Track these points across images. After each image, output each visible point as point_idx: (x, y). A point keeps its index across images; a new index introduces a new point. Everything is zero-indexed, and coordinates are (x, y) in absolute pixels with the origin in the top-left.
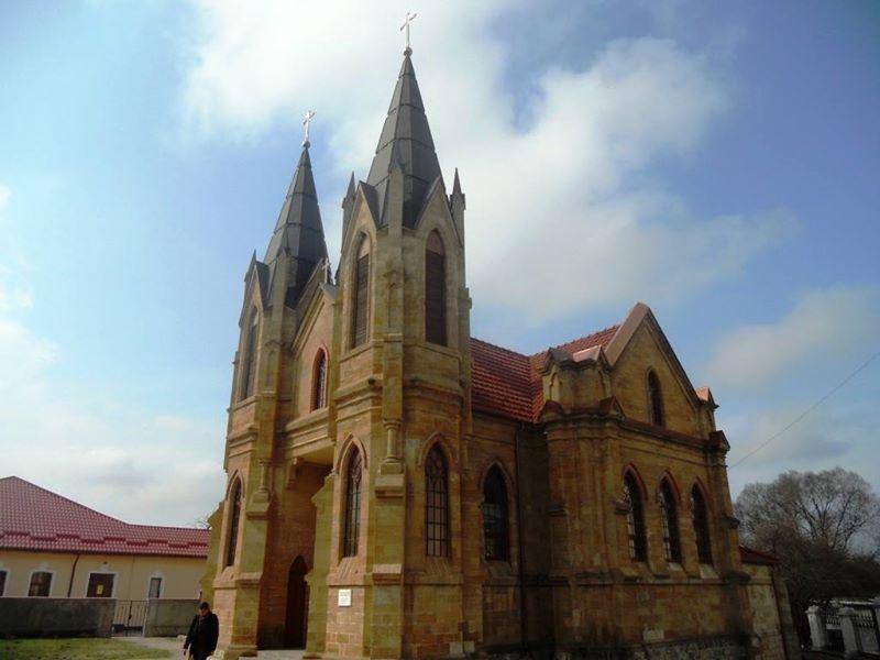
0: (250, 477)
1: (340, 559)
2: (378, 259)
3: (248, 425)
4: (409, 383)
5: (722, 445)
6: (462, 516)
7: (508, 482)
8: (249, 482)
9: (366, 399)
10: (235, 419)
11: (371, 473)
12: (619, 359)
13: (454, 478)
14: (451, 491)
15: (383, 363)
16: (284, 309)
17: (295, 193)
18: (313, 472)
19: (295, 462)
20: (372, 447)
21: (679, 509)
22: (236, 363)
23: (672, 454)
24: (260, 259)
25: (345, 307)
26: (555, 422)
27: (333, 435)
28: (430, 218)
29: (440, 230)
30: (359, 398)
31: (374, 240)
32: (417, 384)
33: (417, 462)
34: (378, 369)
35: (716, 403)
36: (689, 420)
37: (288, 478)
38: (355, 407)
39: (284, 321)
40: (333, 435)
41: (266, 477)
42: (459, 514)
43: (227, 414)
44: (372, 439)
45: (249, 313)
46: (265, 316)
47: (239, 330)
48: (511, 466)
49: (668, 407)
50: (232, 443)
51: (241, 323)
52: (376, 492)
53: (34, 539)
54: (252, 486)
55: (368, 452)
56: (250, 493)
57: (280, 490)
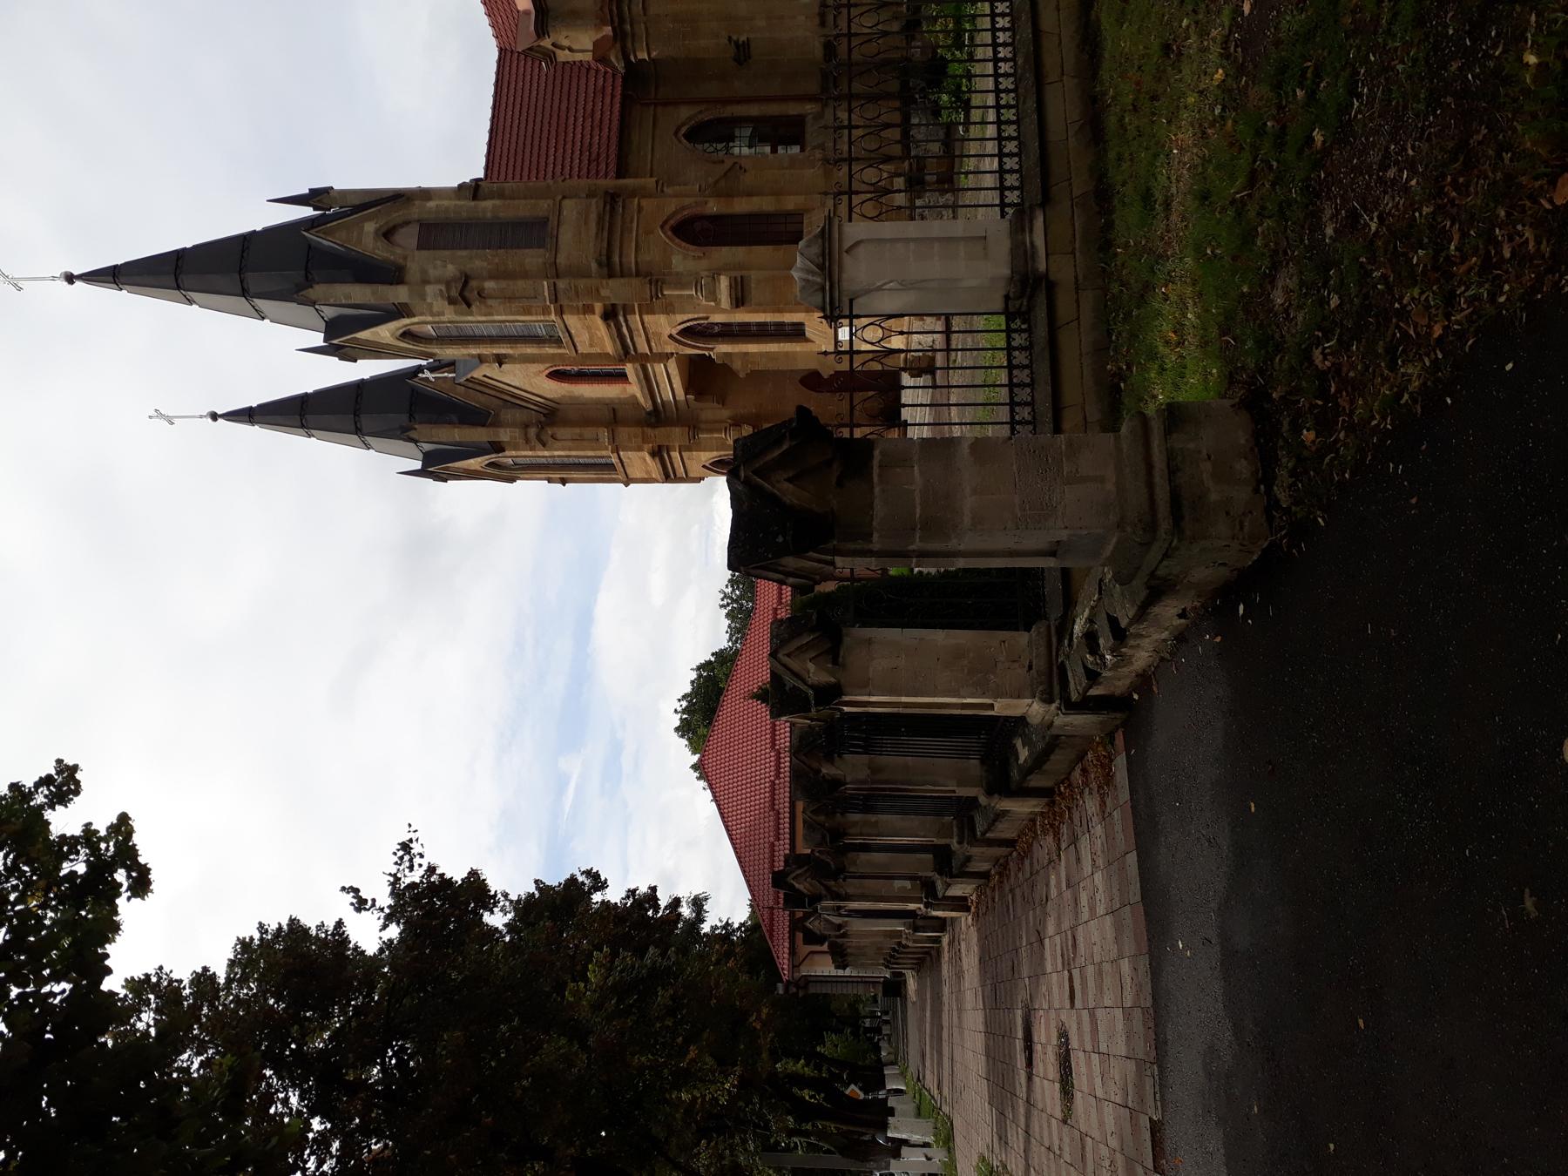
1: (808, 340)
2: (443, 314)
3: (648, 458)
4: (605, 270)
6: (757, 194)
7: (706, 117)
8: (717, 450)
9: (626, 321)
10: (638, 475)
13: (713, 207)
15: (580, 304)
16: (488, 426)
17: (303, 426)
18: (701, 375)
22: (564, 482)
24: (417, 465)
25: (503, 351)
27: (664, 357)
28: (366, 238)
29: (384, 229)
31: (415, 320)
32: (604, 258)
33: (699, 258)
34: (588, 310)
38: (635, 333)
39: (508, 425)
40: (664, 357)
41: (711, 431)
42: (755, 199)
43: (632, 486)
44: (674, 313)
45: (496, 472)
46: (503, 450)
47: (519, 482)
48: (685, 112)
50: (669, 476)
51: (511, 480)
52: (737, 307)
55: (690, 316)
57: (725, 413)
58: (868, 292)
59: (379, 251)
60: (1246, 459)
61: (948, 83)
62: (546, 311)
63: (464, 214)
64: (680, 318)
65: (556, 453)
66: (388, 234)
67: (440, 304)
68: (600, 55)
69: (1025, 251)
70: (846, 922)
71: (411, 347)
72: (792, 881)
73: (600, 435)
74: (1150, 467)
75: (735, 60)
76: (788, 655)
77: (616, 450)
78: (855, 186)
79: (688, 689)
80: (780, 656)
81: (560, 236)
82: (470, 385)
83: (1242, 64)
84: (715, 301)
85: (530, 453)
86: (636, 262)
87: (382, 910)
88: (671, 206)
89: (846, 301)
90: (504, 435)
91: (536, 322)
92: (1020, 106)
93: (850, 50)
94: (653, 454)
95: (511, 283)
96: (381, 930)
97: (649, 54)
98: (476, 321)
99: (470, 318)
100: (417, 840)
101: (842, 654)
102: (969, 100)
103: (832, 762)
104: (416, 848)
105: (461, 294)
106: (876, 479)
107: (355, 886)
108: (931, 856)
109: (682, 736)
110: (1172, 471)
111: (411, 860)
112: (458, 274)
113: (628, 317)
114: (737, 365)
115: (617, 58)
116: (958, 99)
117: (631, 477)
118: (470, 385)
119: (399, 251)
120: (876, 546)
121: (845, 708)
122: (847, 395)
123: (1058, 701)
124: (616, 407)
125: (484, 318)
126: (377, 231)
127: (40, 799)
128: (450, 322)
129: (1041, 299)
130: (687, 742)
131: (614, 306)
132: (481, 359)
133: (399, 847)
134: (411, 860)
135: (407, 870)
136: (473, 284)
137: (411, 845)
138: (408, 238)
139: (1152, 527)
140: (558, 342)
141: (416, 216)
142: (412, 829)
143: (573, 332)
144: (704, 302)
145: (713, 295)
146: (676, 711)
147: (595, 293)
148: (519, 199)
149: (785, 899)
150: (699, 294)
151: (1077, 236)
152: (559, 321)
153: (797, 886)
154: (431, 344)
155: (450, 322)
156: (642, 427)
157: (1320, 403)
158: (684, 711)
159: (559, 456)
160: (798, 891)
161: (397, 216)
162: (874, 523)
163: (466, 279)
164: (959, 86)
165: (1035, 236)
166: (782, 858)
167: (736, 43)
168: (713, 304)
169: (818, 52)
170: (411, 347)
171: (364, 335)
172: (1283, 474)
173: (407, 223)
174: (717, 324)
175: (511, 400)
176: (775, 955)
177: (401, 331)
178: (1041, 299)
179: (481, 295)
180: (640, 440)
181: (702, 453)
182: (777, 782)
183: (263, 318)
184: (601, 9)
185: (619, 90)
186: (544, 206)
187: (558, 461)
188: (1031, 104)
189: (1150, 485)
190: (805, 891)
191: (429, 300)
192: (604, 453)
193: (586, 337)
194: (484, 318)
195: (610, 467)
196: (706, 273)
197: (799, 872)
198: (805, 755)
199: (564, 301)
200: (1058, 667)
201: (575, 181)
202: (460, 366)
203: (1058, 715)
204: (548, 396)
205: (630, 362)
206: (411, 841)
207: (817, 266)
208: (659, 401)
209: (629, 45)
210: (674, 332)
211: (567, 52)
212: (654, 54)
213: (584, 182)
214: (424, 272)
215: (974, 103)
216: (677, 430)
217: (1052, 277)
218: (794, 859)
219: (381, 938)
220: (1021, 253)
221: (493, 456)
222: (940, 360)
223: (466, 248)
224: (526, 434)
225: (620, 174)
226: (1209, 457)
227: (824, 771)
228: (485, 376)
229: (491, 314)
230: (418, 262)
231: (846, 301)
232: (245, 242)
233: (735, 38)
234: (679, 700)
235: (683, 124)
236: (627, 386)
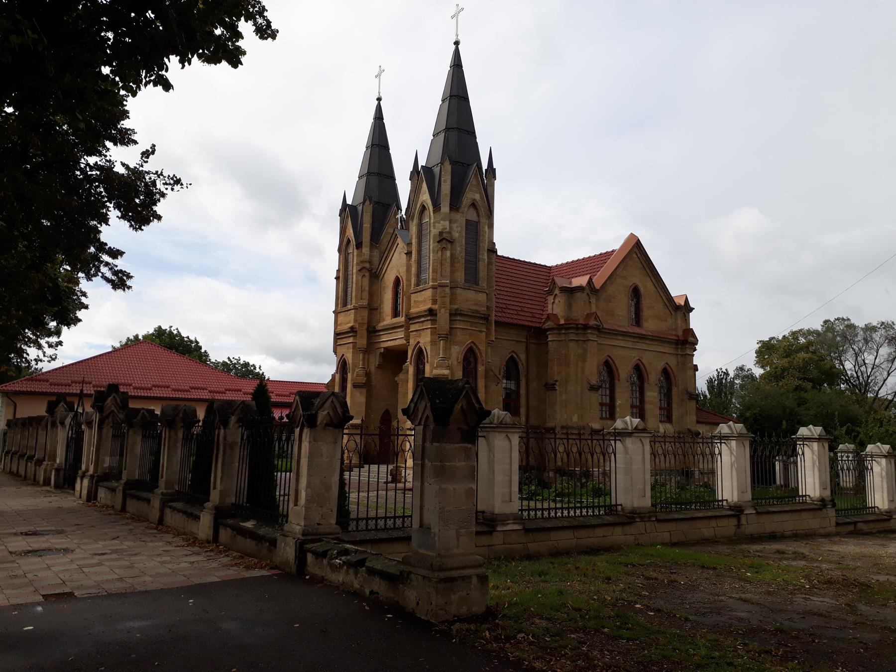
0: (353, 360)
2: (434, 228)
3: (350, 325)
5: (691, 339)
7: (520, 367)
8: (352, 363)
9: (428, 320)
11: (431, 365)
12: (605, 282)
13: (481, 369)
14: (479, 376)
15: (437, 298)
16: (371, 243)
17: (372, 145)
19: (382, 350)
20: (431, 350)
21: (646, 385)
22: (337, 278)
23: (646, 347)
26: (553, 329)
27: (407, 338)
28: (472, 194)
30: (423, 319)
32: (459, 312)
33: (458, 360)
34: (434, 302)
35: (692, 306)
36: (666, 320)
37: (377, 361)
38: (421, 324)
39: (371, 252)
40: (407, 338)
41: (364, 360)
42: (484, 389)
44: (431, 345)
45: (345, 243)
46: (357, 248)
48: (523, 357)
49: (646, 312)
51: (340, 250)
53: (174, 390)
54: (355, 365)
56: (354, 371)
57: (373, 368)
58: (488, 445)
59: (467, 199)
60: (467, 611)
61: (539, 490)
62: (434, 280)
63: (481, 245)
64: (429, 348)
65: (354, 276)
66: (474, 205)
67: (440, 227)
68: (551, 317)
69: (505, 521)
70: (65, 427)
71: (417, 209)
72: (112, 396)
73: (364, 301)
74: (463, 568)
75: (547, 383)
76: (332, 401)
77: (355, 308)
78: (595, 442)
79: (184, 334)
80: (332, 397)
81: (469, 291)
82: (394, 236)
83: (616, 606)
84: (437, 367)
85: (355, 262)
86: (456, 328)
87: (142, 166)
88: (482, 348)
89: (485, 434)
90: (366, 250)
91: (428, 275)
92: (563, 519)
93: (574, 439)
94: (352, 328)
95: (449, 264)
96: (121, 162)
97: (550, 341)
98: (430, 245)
99: (432, 241)
100: (182, 188)
101: (331, 428)
102: (532, 500)
103: (237, 422)
104: (176, 188)
105: (444, 239)
106: (461, 445)
107: (156, 152)
108: (137, 477)
109: (155, 330)
110: (463, 578)
111: (170, 184)
112: (454, 238)
113: (430, 322)
114: (401, 376)
115: (549, 325)
116: (533, 494)
117: (339, 315)
118: (394, 236)
119: (466, 209)
120: (428, 445)
121: (298, 429)
122: (377, 432)
123: (303, 538)
124: (379, 310)
125: (431, 248)
126: (475, 200)
127: (260, 21)
128: (430, 231)
129: (485, 529)
130: (150, 332)
131: (436, 315)
132: (409, 244)
133: (178, 178)
134: (170, 184)
135: (164, 182)
136: (449, 246)
137: (179, 185)
138: (472, 215)
139: (441, 569)
140: (418, 284)
141: (481, 220)
142: (188, 186)
143: (423, 293)
144: (436, 361)
145: (439, 366)
146: (171, 327)
147: (443, 305)
148: (488, 272)
149: (100, 391)
150: (440, 359)
151: (510, 546)
152: (429, 287)
153: (110, 398)
154: (418, 220)
155: (430, 231)
156: (368, 323)
157: (503, 637)
158: (171, 332)
159: (352, 278)
160: (106, 399)
161: (482, 211)
162: (444, 444)
163: (451, 242)
164: (539, 495)
165: (511, 525)
166: (126, 390)
167: (555, 384)
168: (435, 365)
169: (550, 424)
170: (417, 209)
171: (424, 186)
172: (465, 626)
173: (478, 216)
174: (424, 367)
175: (385, 256)
176: (15, 382)
177: (426, 206)
178: (485, 529)
179: (444, 249)
180: (361, 321)
181: (351, 355)
182: (131, 387)
183: (434, 136)
184: (572, 319)
185: (534, 325)
186: (483, 284)
187: (350, 277)
188: (565, 524)
189: (457, 569)
190: (106, 403)
191: (441, 222)
192: (354, 301)
193: (420, 299)
194: (431, 248)
195: (345, 304)
196: (450, 363)
197: (118, 400)
198: (242, 408)
199: (439, 290)
200: (320, 538)
201: (494, 299)
202: (404, 232)
203: (294, 539)
204: (386, 275)
205: (405, 320)
206: (182, 184)
207: (502, 421)
208: (381, 333)
209: (555, 332)
210: (421, 344)
211: (552, 301)
212: (550, 343)
213: (494, 305)
214: (456, 221)
215: (531, 502)
216: (364, 342)
217: (494, 533)
218: (126, 398)
219: (116, 161)
220: (505, 518)
221: (354, 243)
222: (400, 485)
223: (466, 243)
224: (366, 262)
225: (497, 323)
226: (467, 594)
227: (233, 417)
228: (398, 244)
229: (433, 252)
230: (460, 219)
231: (485, 434)
232: (472, 133)
233: (557, 384)
234: (177, 329)
235: (517, 356)
236: (390, 317)
